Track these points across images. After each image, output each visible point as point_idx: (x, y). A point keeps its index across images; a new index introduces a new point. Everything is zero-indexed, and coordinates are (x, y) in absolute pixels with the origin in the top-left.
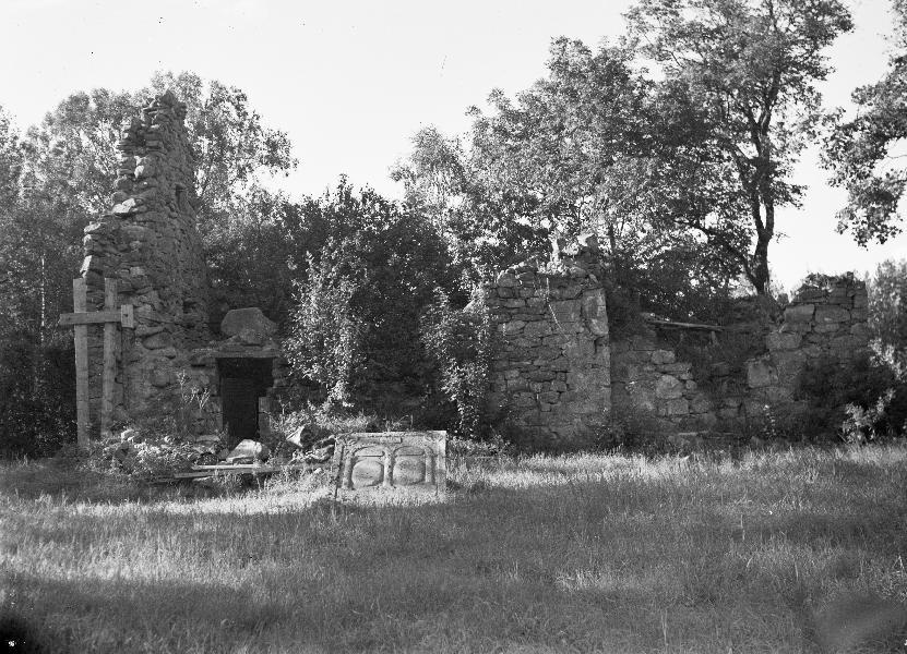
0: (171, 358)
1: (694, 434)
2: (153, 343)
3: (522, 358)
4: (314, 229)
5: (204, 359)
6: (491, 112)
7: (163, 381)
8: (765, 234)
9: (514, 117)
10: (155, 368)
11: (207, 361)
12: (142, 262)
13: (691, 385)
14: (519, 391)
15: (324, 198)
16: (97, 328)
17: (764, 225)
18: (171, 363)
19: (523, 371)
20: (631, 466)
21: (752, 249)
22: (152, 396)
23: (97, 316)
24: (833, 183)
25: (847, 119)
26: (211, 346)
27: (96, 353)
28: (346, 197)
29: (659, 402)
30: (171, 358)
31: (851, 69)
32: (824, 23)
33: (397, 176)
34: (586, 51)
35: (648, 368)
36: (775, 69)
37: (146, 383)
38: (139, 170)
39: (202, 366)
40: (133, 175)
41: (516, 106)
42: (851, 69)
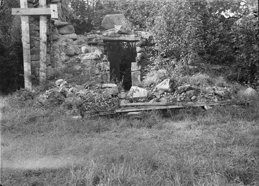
0: (74, 40)
2: (63, 30)
7: (73, 52)
10: (67, 45)
16: (35, 19)
20: (170, 135)
22: (66, 61)
23: (34, 11)
26: (99, 34)
27: (34, 33)
30: (74, 40)
39: (95, 44)
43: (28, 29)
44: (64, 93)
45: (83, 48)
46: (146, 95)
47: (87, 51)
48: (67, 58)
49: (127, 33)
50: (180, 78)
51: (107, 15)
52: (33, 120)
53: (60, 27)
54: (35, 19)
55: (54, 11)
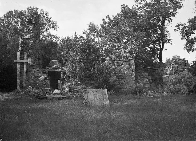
0: (38, 71)
1: (153, 91)
3: (116, 74)
4: (70, 44)
5: (46, 71)
6: (107, 20)
7: (37, 75)
8: (162, 49)
9: (112, 21)
10: (35, 73)
11: (46, 72)
12: (31, 49)
13: (151, 81)
14: (116, 81)
15: (71, 37)
17: (162, 47)
18: (38, 72)
19: (117, 76)
21: (159, 52)
22: (34, 79)
24: (182, 39)
25: (186, 25)
26: (47, 68)
28: (76, 37)
29: (144, 84)
30: (38, 71)
31: (183, 16)
32: (177, 5)
33: (84, 33)
34: (129, 8)
35: (142, 77)
36: (167, 15)
37: (33, 76)
38: (31, 29)
40: (29, 29)
41: (112, 18)
42: (183, 16)
43: (20, 67)
44: (30, 91)
45: (40, 75)
46: (59, 93)
47: (41, 76)
48: (34, 78)
49: (59, 68)
50: (73, 86)
51: (52, 61)
52: (17, 99)
53: (32, 66)
54: (22, 64)
55: (29, 61)
